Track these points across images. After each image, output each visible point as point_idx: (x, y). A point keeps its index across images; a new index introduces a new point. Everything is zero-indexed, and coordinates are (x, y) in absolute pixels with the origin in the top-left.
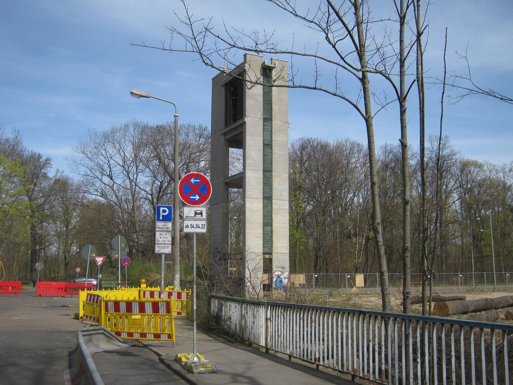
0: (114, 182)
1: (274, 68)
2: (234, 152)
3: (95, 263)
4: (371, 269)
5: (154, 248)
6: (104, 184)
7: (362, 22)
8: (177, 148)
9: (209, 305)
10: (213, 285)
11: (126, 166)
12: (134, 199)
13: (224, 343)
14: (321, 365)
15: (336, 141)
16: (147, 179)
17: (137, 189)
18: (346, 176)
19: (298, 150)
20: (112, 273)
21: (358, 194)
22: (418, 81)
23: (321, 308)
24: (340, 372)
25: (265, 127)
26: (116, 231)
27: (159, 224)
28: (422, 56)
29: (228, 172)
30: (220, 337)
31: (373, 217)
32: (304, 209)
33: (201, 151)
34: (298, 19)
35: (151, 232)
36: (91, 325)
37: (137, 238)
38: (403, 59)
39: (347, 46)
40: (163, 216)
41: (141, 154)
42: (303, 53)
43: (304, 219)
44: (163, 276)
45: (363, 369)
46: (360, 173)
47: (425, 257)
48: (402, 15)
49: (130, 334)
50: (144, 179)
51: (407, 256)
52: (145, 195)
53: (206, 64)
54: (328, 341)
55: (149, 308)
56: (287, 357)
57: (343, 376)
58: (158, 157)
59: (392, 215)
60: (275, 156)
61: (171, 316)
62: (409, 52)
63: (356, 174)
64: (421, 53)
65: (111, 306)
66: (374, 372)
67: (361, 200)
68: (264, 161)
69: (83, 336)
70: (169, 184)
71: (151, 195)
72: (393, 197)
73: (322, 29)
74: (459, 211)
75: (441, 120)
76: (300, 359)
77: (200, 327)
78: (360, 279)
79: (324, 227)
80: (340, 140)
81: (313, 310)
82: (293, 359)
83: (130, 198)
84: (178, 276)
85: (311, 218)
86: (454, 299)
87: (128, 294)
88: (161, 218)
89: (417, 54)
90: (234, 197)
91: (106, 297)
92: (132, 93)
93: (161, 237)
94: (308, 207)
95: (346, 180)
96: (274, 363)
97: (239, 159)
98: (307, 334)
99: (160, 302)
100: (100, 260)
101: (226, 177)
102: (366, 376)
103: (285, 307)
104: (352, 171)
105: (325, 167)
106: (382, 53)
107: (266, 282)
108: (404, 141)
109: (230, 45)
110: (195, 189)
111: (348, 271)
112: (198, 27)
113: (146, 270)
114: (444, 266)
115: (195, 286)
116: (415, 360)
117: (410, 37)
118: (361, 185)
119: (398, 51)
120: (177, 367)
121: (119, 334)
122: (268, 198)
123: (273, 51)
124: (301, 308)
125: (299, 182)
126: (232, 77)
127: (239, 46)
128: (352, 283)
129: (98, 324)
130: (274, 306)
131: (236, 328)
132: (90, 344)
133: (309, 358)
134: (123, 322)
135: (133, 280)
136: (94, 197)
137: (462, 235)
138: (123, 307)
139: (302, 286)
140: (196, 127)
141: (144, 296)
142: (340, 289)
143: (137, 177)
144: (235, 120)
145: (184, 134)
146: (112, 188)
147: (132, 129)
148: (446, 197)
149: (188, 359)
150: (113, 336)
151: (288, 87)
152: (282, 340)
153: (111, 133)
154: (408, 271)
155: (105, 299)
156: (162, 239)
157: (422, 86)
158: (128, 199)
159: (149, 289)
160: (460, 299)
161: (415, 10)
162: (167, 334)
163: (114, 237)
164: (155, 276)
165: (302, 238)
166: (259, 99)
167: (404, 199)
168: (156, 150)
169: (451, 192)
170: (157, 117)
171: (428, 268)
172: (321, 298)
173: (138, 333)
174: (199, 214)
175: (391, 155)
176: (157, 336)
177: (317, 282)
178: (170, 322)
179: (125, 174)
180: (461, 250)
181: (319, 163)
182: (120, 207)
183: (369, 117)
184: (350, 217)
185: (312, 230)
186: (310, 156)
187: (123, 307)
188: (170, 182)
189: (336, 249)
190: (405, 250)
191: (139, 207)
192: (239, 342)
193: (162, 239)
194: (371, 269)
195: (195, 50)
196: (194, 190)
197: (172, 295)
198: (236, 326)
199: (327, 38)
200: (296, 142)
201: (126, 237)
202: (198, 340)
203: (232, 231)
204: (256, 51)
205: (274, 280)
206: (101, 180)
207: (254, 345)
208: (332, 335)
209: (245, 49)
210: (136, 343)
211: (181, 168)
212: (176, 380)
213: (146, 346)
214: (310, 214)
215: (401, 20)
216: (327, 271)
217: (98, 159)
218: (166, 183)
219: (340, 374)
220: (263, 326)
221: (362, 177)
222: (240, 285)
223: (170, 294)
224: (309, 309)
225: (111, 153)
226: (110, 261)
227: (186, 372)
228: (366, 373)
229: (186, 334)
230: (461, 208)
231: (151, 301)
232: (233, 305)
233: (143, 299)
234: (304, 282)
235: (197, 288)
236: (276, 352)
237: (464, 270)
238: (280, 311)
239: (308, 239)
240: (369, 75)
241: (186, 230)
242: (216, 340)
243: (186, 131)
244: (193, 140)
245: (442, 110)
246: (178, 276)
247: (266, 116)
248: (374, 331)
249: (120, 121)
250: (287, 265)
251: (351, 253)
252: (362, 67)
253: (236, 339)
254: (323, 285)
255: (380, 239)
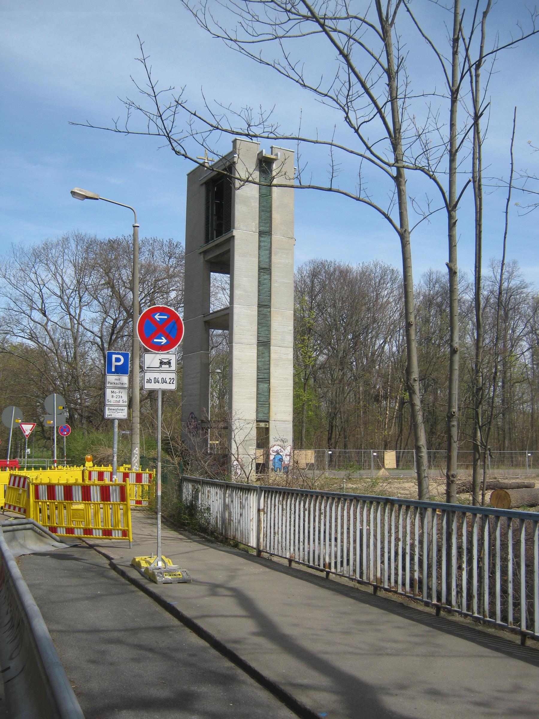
0: (48, 320)
1: (275, 160)
2: (218, 279)
3: (22, 433)
4: (407, 445)
5: (103, 411)
6: (35, 322)
7: (396, 98)
8: (137, 271)
9: (180, 490)
10: (186, 463)
11: (65, 297)
12: (76, 345)
13: (200, 543)
14: (333, 573)
15: (361, 265)
16: (94, 315)
17: (81, 329)
18: (374, 314)
19: (309, 277)
20: (45, 447)
21: (390, 339)
22: (474, 182)
23: (333, 494)
24: (359, 582)
25: (262, 244)
26: (51, 389)
27: (111, 378)
28: (480, 146)
29: (209, 307)
30: (195, 535)
31: (409, 372)
32: (315, 360)
33: (170, 277)
34: (307, 91)
35: (101, 389)
36: (16, 518)
37: (80, 398)
38: (454, 150)
39: (375, 130)
40: (116, 366)
41: (87, 279)
42: (314, 139)
43: (314, 373)
44: (115, 450)
45: (389, 579)
46: (394, 312)
47: (477, 426)
48: (454, 89)
49: (70, 531)
50: (90, 315)
51: (453, 426)
52: (92, 337)
53: (177, 153)
54: (342, 542)
55: (96, 494)
56: (286, 562)
57: (363, 588)
58: (110, 284)
59: (437, 370)
60: (275, 286)
61: (126, 505)
62: (462, 141)
63: (388, 313)
64: (479, 142)
65: (43, 490)
66: (404, 584)
67: (394, 349)
68: (259, 292)
69: (4, 532)
70: (126, 322)
71: (101, 338)
72: (439, 346)
73: (341, 106)
74: (530, 366)
75: (505, 238)
76: (304, 564)
77: (167, 520)
78: (390, 458)
79: (342, 386)
80: (366, 264)
81: (322, 497)
82: (294, 565)
83: (71, 341)
84: (137, 451)
85: (324, 372)
86: (519, 487)
87: (68, 475)
88: (113, 370)
89: (474, 144)
90: (217, 342)
91: (36, 479)
92: (73, 193)
93: (113, 396)
94: (320, 358)
95: (375, 321)
96: (268, 570)
97: (224, 289)
98: (314, 531)
99: (112, 485)
100: (28, 428)
101: (206, 313)
102: (393, 587)
103: (284, 493)
104: (383, 307)
105: (344, 302)
106: (424, 142)
107: (261, 461)
108: (452, 265)
109: (212, 126)
110: (160, 329)
111: (373, 446)
112: (165, 100)
113: (93, 443)
114: (507, 442)
115: (160, 464)
116: (460, 568)
117: (464, 119)
118: (395, 327)
119: (447, 139)
120: (134, 574)
121: (54, 530)
122: (264, 344)
123: (271, 135)
124: (307, 495)
125: (309, 323)
126: (215, 173)
127: (224, 128)
128: (380, 463)
129: (24, 517)
130: (269, 492)
131: (217, 523)
132: (14, 543)
133: (316, 563)
134: (60, 513)
135: (74, 457)
136: (19, 339)
137: (532, 399)
138: (60, 492)
139: (310, 466)
140: (165, 242)
141: (90, 479)
142: (362, 472)
143: (80, 312)
144: (219, 233)
145: (147, 253)
146: (45, 327)
147: (73, 245)
148: (512, 346)
149: (150, 564)
150: (46, 532)
151: (292, 187)
152: (280, 538)
153: (44, 250)
154: (455, 446)
155: (34, 482)
156: (115, 399)
157: (480, 189)
158: (68, 344)
159: (97, 468)
160: (527, 487)
161: (471, 82)
162: (121, 530)
163: (47, 396)
164: (104, 451)
165: (311, 401)
166: (253, 204)
167: (451, 346)
168: (107, 274)
169: (519, 339)
170: (109, 228)
171: (482, 443)
172: (336, 483)
173: (80, 528)
174: (165, 363)
175: (437, 285)
176: (107, 533)
177: (331, 461)
178: (126, 514)
179: (64, 307)
180: (530, 419)
181: (337, 296)
182: (57, 354)
183: (405, 231)
184: (378, 372)
185: (326, 390)
186: (324, 286)
187: (60, 492)
188: (127, 319)
189: (359, 416)
190: (450, 416)
191: (84, 355)
192: (221, 542)
193: (115, 399)
194: (407, 445)
195: (161, 133)
196: (158, 330)
197: (128, 477)
198: (217, 520)
199: (347, 118)
200: (304, 266)
201: (65, 397)
202: (164, 538)
203: (213, 390)
204: (247, 135)
205: (272, 457)
206: (30, 317)
207: (242, 546)
208: (348, 533)
209: (233, 133)
210: (78, 542)
211: (143, 301)
212: (133, 592)
213: (91, 547)
214: (322, 367)
215: (452, 96)
216: (345, 447)
217: (25, 286)
218: (122, 322)
219: (357, 585)
220: (254, 519)
221: (397, 316)
222: (223, 464)
223: (126, 476)
224: (317, 497)
225: (43, 278)
226: (43, 430)
227: (146, 581)
228: (393, 584)
229: (147, 530)
230: (532, 362)
231: (99, 485)
232: (213, 490)
233: (87, 482)
234: (313, 461)
235: (162, 467)
236: (271, 555)
237: (535, 447)
238: (277, 499)
239: (319, 402)
240: (406, 172)
241: (148, 386)
242: (189, 539)
243: (151, 248)
244: (159, 261)
245: (506, 224)
246: (137, 451)
247: (263, 229)
248: (405, 527)
249: (55, 232)
250: (290, 437)
251: (379, 422)
252: (397, 160)
253: (216, 538)
254: (339, 466)
255: (417, 401)
